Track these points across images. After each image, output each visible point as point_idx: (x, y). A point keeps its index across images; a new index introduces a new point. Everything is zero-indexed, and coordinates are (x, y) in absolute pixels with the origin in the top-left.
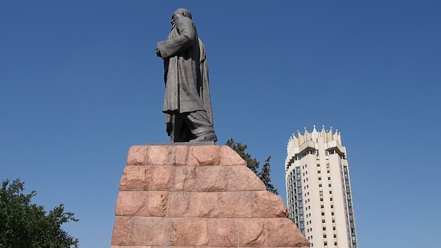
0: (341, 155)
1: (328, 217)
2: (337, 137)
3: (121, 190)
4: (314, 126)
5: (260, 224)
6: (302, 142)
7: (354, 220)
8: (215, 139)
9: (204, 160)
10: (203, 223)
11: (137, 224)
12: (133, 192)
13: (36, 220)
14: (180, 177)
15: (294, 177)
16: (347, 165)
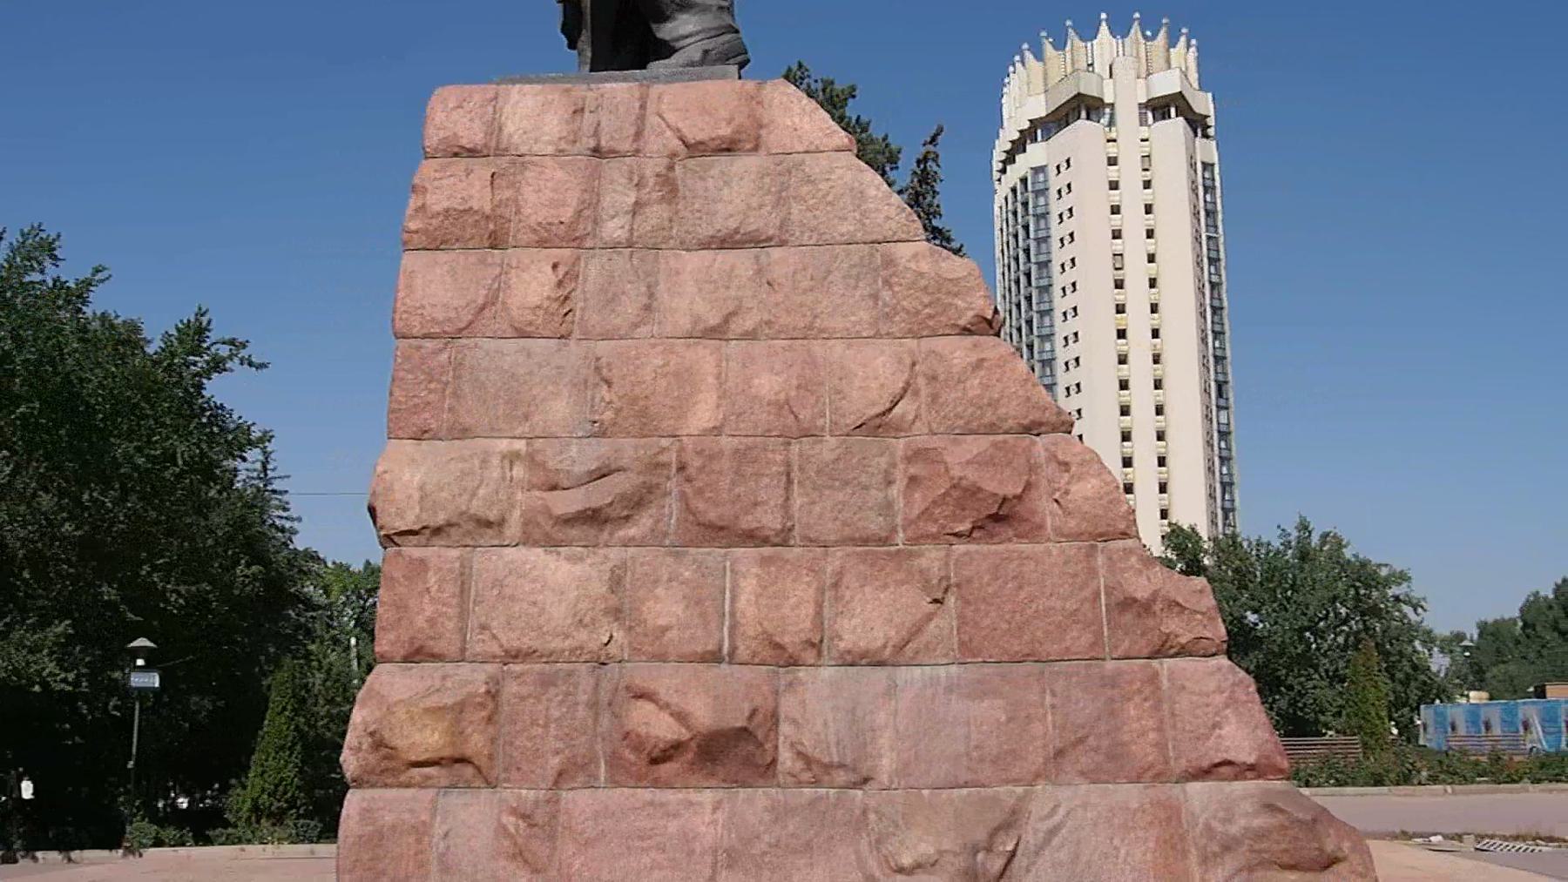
0: (1197, 124)
1: (1139, 345)
2: (1185, 56)
3: (407, 247)
4: (1104, 16)
5: (900, 361)
6: (1055, 77)
7: (1228, 353)
8: (740, 58)
9: (701, 137)
10: (704, 357)
11: (472, 367)
12: (452, 255)
13: (116, 366)
14: (618, 194)
15: (1025, 204)
16: (1216, 160)
